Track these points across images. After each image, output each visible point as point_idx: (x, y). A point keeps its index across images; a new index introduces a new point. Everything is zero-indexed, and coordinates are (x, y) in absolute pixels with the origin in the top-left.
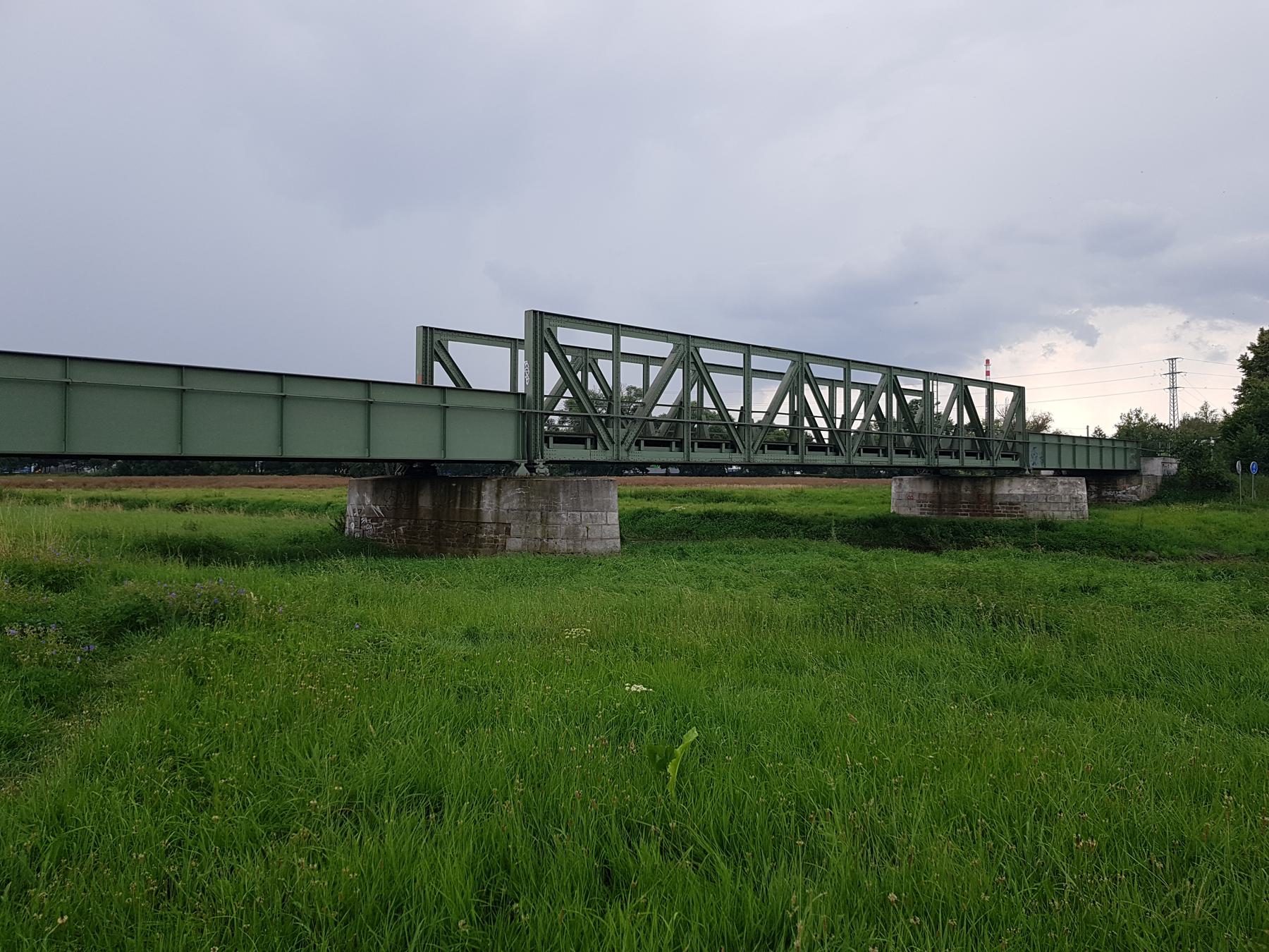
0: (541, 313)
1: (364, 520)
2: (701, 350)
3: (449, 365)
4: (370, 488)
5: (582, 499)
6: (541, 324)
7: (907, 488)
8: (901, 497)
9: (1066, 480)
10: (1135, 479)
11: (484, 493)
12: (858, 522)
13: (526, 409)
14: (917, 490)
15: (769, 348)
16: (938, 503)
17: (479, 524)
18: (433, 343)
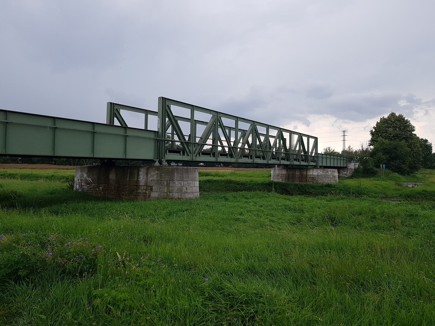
0: (165, 98)
1: (83, 184)
2: (222, 118)
3: (120, 119)
4: (86, 170)
5: (184, 176)
6: (165, 103)
7: (277, 172)
8: (275, 175)
9: (331, 170)
10: (346, 170)
11: (140, 173)
12: (262, 184)
13: (158, 138)
14: (281, 173)
15: (244, 119)
16: (288, 177)
17: (138, 186)
18: (114, 109)
